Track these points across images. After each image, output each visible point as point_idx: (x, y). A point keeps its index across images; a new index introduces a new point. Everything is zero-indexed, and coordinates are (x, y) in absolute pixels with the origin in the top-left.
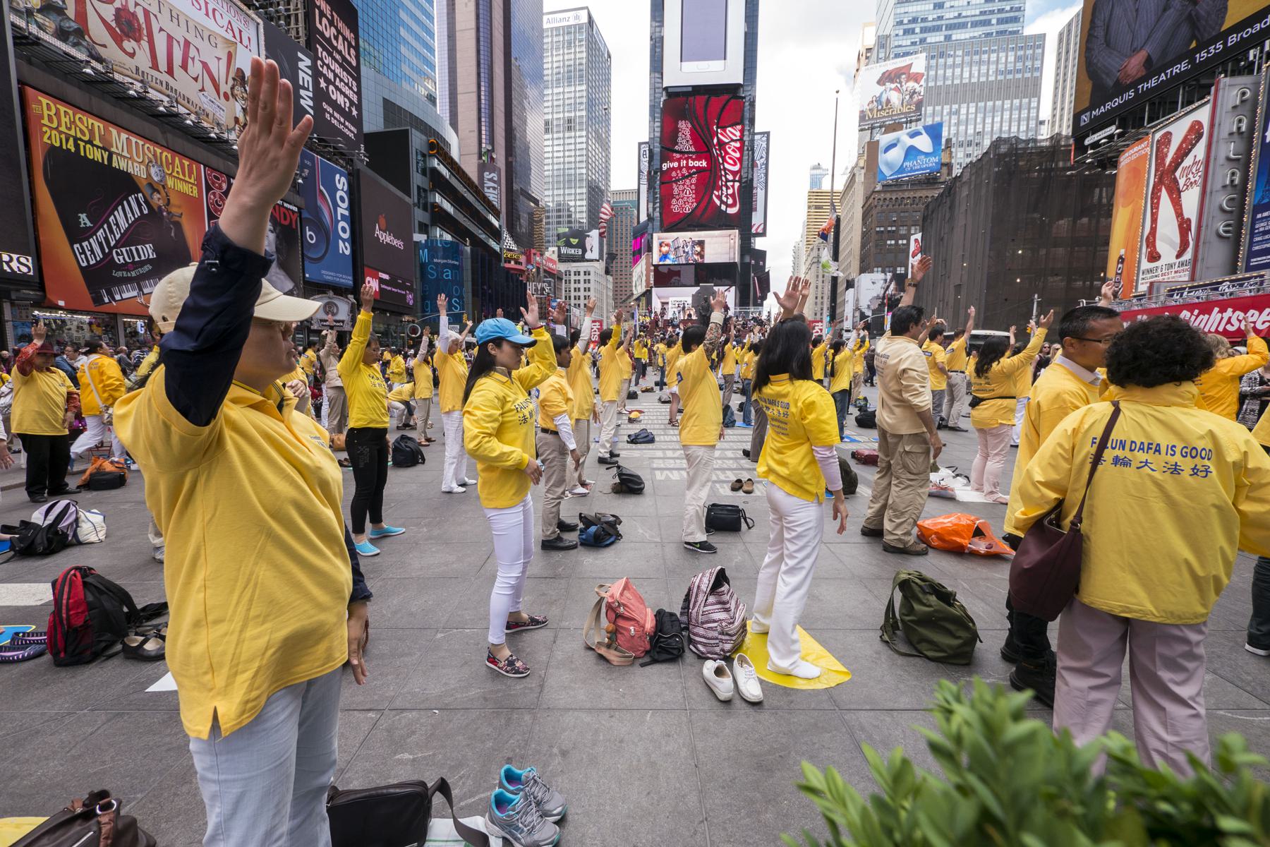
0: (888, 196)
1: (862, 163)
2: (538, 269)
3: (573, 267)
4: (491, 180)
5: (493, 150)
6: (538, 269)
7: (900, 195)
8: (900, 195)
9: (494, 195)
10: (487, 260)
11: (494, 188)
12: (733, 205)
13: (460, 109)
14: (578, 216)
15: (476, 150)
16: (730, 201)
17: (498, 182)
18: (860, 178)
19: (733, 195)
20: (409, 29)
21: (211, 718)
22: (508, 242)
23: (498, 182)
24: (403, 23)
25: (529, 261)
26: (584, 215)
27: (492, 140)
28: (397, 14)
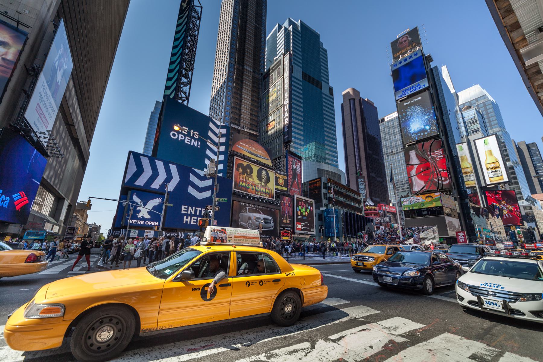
5: (361, 171)
15: (355, 172)
23: (364, 181)
25: (380, 209)
27: (361, 167)
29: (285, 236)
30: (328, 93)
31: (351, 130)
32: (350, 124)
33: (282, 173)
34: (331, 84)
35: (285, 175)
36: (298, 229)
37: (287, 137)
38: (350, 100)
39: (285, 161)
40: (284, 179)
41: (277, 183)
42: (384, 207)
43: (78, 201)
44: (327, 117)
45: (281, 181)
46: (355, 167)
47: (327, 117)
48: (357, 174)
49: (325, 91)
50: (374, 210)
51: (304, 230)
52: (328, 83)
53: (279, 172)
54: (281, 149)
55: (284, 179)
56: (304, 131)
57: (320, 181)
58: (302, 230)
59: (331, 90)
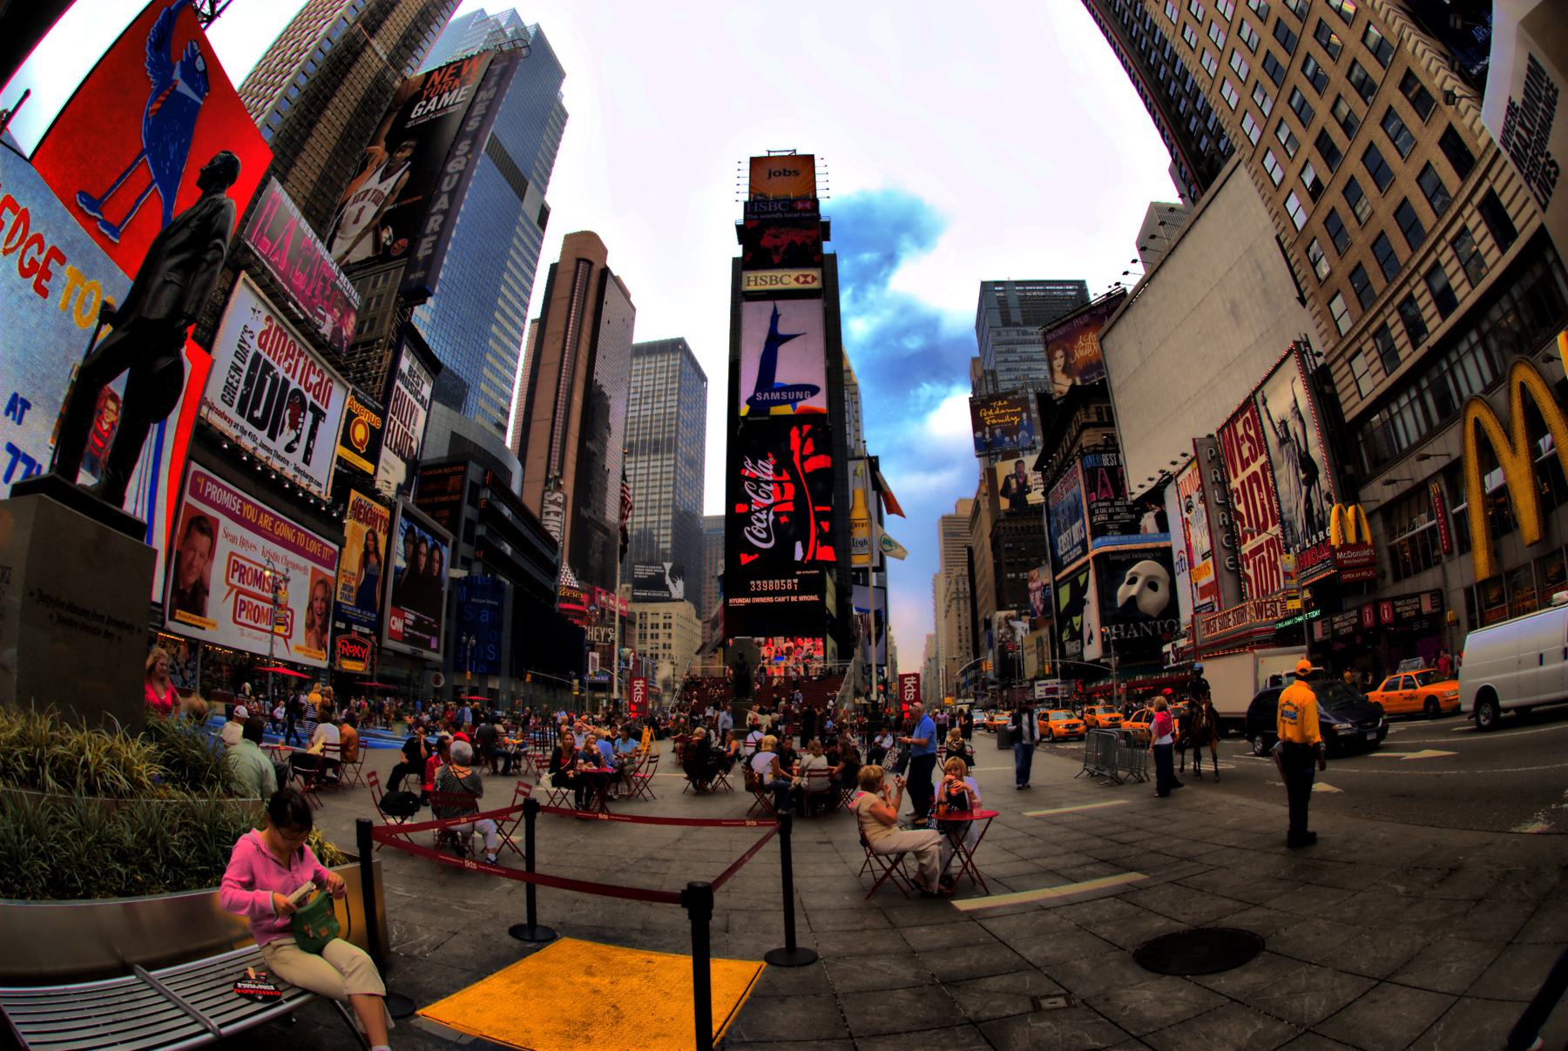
0: (1013, 525)
1: (984, 490)
2: (603, 610)
3: (649, 608)
4: (554, 502)
5: (561, 476)
6: (603, 610)
7: (1025, 524)
8: (1025, 524)
9: (557, 525)
10: (536, 598)
11: (557, 514)
12: (767, 540)
13: (533, 435)
14: (661, 546)
15: (543, 477)
16: (764, 536)
17: (564, 505)
18: (985, 506)
19: (767, 529)
20: (522, 227)
21: (529, 460)
22: (567, 578)
23: (564, 505)
24: (497, 323)
25: (592, 601)
26: (669, 545)
27: (561, 468)
28: (498, 287)
29: (350, 658)
30: (535, 218)
31: (559, 344)
32: (562, 329)
33: (369, 400)
34: (549, 199)
35: (376, 411)
36: (394, 635)
37: (419, 274)
38: (579, 260)
39: (387, 361)
40: (372, 429)
41: (346, 441)
42: (603, 598)
43: (1179, 201)
44: (511, 282)
45: (360, 433)
46: (545, 460)
47: (511, 282)
48: (547, 481)
49: (530, 208)
50: (577, 601)
51: (410, 640)
52: (544, 193)
53: (361, 394)
54: (384, 315)
55: (372, 429)
56: (505, 269)
57: (464, 473)
58: (405, 641)
59: (544, 214)
